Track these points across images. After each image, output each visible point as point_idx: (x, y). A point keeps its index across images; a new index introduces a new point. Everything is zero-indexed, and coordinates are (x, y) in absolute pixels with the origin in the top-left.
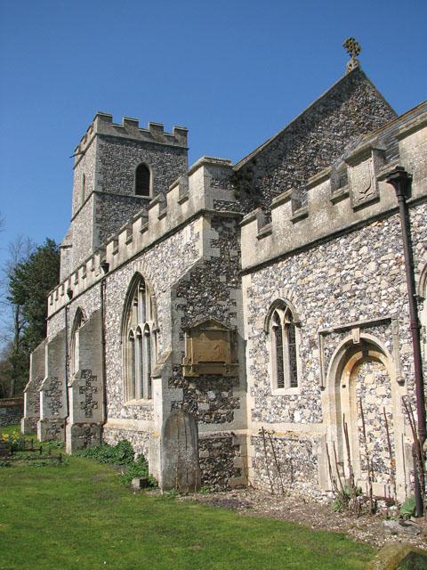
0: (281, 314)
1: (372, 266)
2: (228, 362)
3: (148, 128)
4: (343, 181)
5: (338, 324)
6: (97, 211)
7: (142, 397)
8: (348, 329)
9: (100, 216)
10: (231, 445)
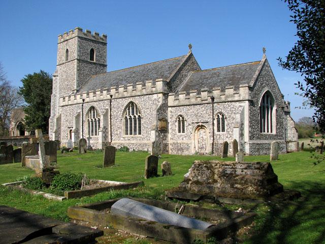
1: (205, 112)
3: (94, 34)
5: (196, 122)
6: (78, 67)
7: (131, 134)
9: (79, 68)
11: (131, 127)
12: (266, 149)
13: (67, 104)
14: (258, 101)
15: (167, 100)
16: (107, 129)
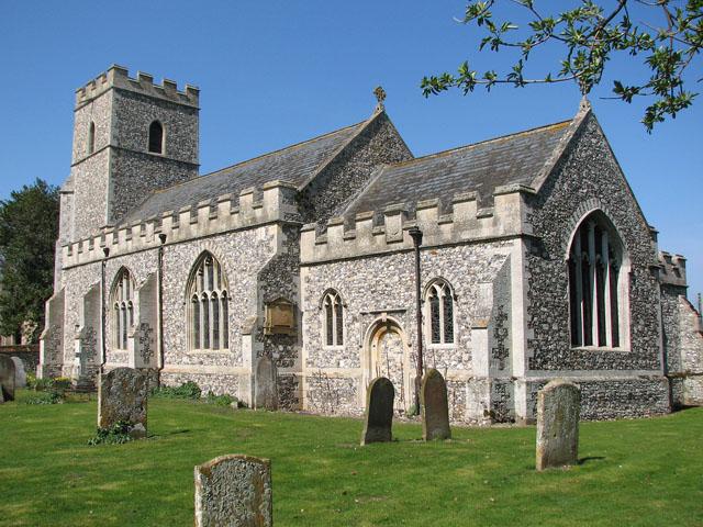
0: (332, 298)
1: (396, 278)
2: (291, 326)
3: (162, 85)
4: (380, 222)
6: (112, 166)
7: (207, 346)
8: (380, 313)
9: (115, 171)
10: (293, 382)
11: (207, 329)
12: (594, 399)
13: (76, 263)
14: (559, 242)
15: (298, 246)
16: (151, 330)
